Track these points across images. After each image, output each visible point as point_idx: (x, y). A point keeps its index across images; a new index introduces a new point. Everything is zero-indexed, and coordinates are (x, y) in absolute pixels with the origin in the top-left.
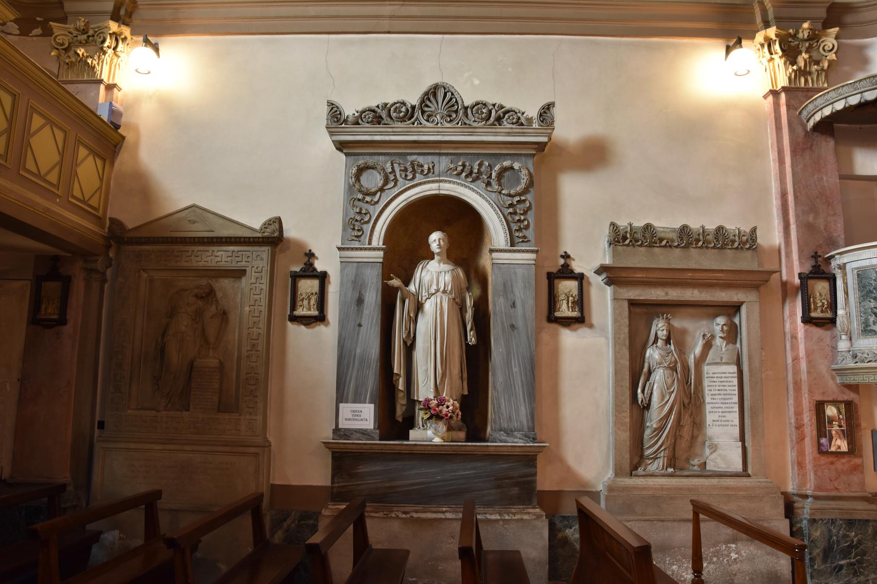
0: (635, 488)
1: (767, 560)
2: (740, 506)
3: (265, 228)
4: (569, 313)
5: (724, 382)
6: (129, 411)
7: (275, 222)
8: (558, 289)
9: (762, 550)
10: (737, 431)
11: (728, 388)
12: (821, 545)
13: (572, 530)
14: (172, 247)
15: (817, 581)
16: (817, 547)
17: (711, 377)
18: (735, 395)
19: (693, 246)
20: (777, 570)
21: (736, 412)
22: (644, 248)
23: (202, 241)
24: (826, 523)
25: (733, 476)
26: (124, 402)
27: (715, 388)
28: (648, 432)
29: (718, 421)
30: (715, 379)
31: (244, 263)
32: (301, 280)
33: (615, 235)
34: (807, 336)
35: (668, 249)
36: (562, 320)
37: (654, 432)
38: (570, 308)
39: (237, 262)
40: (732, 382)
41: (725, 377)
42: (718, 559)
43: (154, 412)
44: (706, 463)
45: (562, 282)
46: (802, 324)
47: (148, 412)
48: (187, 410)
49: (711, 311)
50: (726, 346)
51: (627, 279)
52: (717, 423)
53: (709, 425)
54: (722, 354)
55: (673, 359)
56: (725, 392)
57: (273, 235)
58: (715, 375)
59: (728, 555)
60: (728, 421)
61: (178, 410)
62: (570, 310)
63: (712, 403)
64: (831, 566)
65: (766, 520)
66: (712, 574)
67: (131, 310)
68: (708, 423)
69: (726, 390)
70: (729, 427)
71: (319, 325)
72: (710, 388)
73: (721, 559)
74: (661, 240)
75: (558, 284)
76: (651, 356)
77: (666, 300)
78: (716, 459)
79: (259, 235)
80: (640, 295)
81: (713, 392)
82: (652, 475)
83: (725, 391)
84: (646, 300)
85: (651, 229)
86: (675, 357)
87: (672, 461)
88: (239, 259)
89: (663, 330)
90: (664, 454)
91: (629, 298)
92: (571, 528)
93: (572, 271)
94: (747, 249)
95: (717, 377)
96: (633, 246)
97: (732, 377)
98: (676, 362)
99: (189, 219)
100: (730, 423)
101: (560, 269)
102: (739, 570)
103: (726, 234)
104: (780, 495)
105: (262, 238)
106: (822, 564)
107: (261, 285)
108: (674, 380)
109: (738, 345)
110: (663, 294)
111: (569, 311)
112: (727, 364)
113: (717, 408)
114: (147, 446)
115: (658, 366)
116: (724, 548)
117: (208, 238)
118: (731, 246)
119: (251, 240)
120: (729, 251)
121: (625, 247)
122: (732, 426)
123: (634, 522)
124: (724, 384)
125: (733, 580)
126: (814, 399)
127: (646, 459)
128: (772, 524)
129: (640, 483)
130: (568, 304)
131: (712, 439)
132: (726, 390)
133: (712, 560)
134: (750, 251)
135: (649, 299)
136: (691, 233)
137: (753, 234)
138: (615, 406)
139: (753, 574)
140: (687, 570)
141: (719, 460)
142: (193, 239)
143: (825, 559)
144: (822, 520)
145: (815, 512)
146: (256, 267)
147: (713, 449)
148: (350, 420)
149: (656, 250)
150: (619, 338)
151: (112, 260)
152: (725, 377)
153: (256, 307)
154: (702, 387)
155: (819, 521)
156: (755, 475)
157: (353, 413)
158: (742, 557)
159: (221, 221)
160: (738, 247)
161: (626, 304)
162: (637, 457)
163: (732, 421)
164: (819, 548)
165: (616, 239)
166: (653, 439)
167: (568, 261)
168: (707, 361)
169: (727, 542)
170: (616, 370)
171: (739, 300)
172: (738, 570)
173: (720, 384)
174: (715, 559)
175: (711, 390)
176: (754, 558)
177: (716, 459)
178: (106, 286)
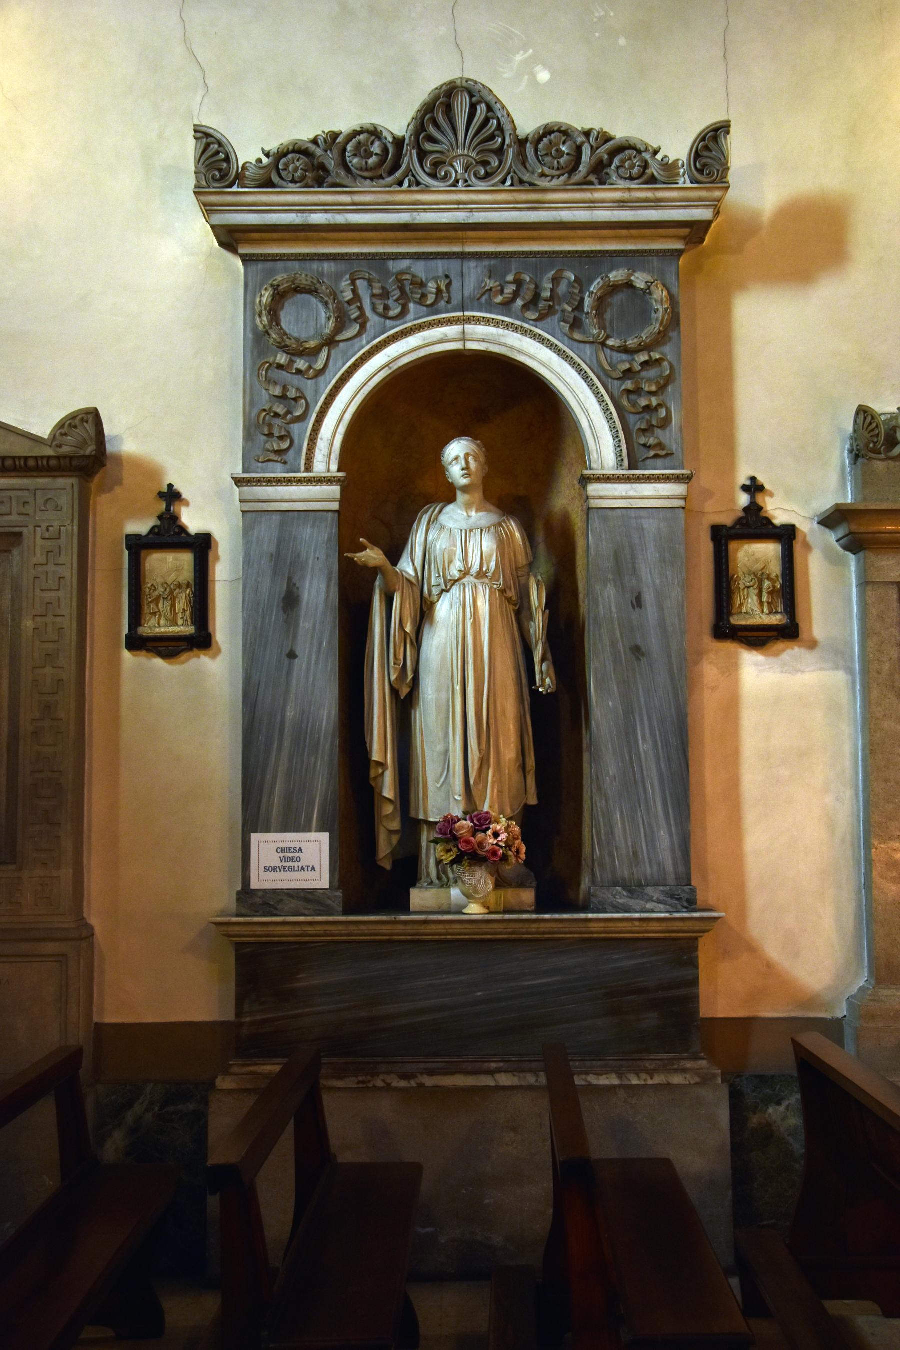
7: (87, 422)
8: (736, 559)
13: (782, 1109)
31: (14, 518)
45: (746, 547)
79: (49, 452)
92: (779, 1104)
93: (768, 521)
101: (741, 519)
111: (763, 612)
121: (890, 462)
130: (760, 596)
146: (44, 526)
148: (274, 869)
150: (879, 673)
153: (50, 619)
157: (282, 855)
165: (871, 446)
167: (760, 499)
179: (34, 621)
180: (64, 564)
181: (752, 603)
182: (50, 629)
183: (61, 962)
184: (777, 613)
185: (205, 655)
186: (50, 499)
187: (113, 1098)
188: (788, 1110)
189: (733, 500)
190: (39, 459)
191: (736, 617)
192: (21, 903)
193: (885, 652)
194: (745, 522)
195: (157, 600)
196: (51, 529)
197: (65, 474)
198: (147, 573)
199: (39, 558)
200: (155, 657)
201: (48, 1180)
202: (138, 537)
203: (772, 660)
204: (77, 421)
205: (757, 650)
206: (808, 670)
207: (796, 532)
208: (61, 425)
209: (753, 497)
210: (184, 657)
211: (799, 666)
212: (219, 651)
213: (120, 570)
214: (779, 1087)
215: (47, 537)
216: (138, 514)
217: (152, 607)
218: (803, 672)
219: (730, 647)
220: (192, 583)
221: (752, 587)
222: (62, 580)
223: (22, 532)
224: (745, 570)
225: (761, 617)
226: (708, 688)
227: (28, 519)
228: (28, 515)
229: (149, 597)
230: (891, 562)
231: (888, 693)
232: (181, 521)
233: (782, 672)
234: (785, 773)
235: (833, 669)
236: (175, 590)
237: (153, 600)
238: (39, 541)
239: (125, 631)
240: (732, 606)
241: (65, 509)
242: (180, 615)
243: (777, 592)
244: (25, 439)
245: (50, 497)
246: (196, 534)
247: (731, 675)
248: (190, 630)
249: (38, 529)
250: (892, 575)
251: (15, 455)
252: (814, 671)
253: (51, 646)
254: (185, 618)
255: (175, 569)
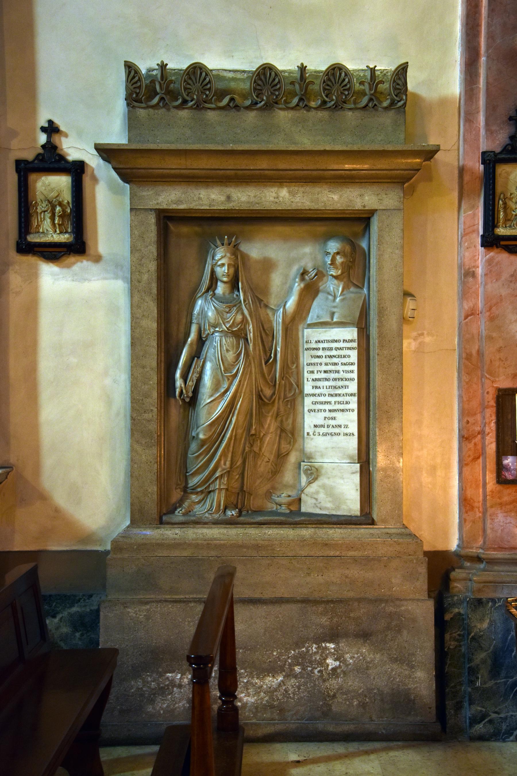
0: (160, 545)
1: (392, 670)
2: (346, 577)
4: (55, 236)
5: (335, 356)
8: (35, 188)
9: (382, 655)
10: (352, 444)
11: (340, 368)
12: (490, 645)
13: (56, 620)
15: (479, 708)
16: (481, 648)
17: (314, 349)
18: (352, 380)
19: (280, 106)
20: (409, 689)
21: (353, 410)
22: (186, 111)
24: (500, 606)
25: (342, 524)
27: (319, 368)
28: (194, 446)
29: (323, 426)
30: (320, 353)
33: (132, 88)
34: (491, 271)
35: (233, 113)
37: (202, 446)
38: (57, 226)
40: (349, 356)
41: (337, 349)
42: (303, 669)
44: (300, 500)
45: (43, 178)
46: (483, 248)
49: (321, 228)
50: (343, 291)
51: (151, 170)
52: (322, 430)
53: (308, 434)
54: (335, 307)
55: (239, 317)
56: (336, 376)
58: (321, 345)
59: (322, 663)
60: (340, 426)
62: (58, 232)
63: (314, 395)
64: (505, 683)
65: (392, 601)
66: (291, 695)
68: (307, 430)
69: (338, 372)
70: (341, 437)
72: (311, 368)
73: (309, 669)
74: (221, 94)
75: (35, 181)
76: (202, 312)
77: (227, 210)
78: (317, 493)
80: (179, 201)
81: (316, 376)
82: (198, 523)
83: (337, 374)
84: (190, 210)
85: (270, 74)
86: (243, 314)
87: (240, 497)
89: (223, 265)
90: (220, 485)
91: (158, 207)
92: (54, 617)
93: (62, 158)
94: (386, 108)
95: (324, 349)
96: (165, 106)
97: (349, 349)
98: (244, 320)
100: (343, 430)
101: (39, 154)
102: (340, 688)
103: (347, 80)
104: (421, 556)
106: (491, 680)
108: (239, 355)
109: (365, 290)
110: (223, 198)
111: (56, 231)
112: (341, 324)
113: (322, 403)
115: (212, 330)
116: (314, 650)
118: (355, 103)
120: (350, 113)
121: (151, 110)
122: (347, 434)
123: (154, 604)
124: (335, 360)
125: (330, 706)
126: (495, 386)
127: (192, 493)
128: (403, 608)
129: (172, 536)
130: (53, 218)
131: (312, 458)
132: (338, 372)
133: (292, 670)
134: (391, 113)
135: (197, 208)
136: (277, 80)
137: (399, 79)
138: (132, 402)
139: (366, 696)
140: (247, 689)
141: (322, 496)
143: (495, 672)
144: (493, 600)
145: (484, 587)
147: (313, 477)
149: (211, 115)
150: (139, 282)
152: (337, 349)
154: (297, 367)
155: (488, 602)
156: (384, 521)
158: (347, 666)
160: (367, 105)
161: (152, 219)
162: (179, 490)
163: (346, 426)
164: (486, 651)
165: (134, 96)
166: (202, 457)
167: (56, 139)
168: (309, 321)
169: (319, 640)
170: (133, 338)
171: (364, 206)
172: (338, 689)
173: (328, 360)
174: (297, 669)
175: (312, 372)
176: (368, 668)
177: (317, 493)
181: (47, 224)
184: (66, 232)
188: (61, 622)
189: (35, 140)
191: (32, 236)
193: (144, 265)
202: (26, 162)
203: (65, 271)
205: (53, 263)
206: (93, 279)
207: (85, 167)
209: (49, 137)
211: (87, 276)
214: (54, 604)
218: (90, 280)
219: (31, 259)
221: (47, 211)
224: (42, 197)
225: (52, 236)
226: (13, 293)
230: (151, 192)
231: (146, 298)
233: (73, 281)
234: (73, 360)
235: (114, 279)
240: (31, 227)
243: (68, 215)
246: (73, 161)
247: (32, 282)
250: (151, 203)
252: (98, 280)
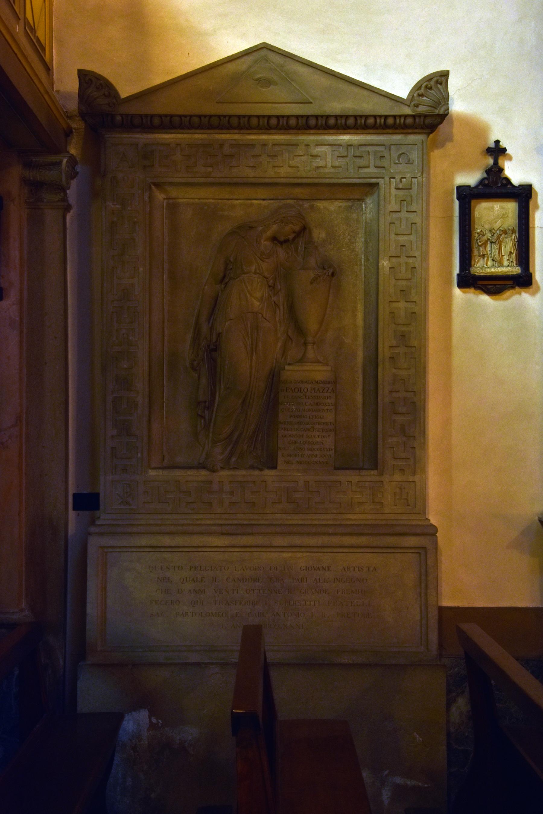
3: (419, 95)
6: (152, 473)
7: (441, 84)
14: (217, 136)
23: (285, 123)
26: (139, 455)
31: (372, 170)
32: (480, 203)
36: (486, 283)
39: (360, 167)
43: (203, 472)
47: (191, 472)
48: (274, 467)
57: (437, 111)
61: (252, 467)
67: (141, 269)
71: (520, 294)
79: (407, 111)
88: (362, 162)
99: (257, 76)
105: (414, 117)
107: (411, 215)
114: (197, 541)
117: (297, 117)
119: (390, 121)
142: (266, 120)
146: (398, 177)
151: (76, 163)
153: (403, 260)
159: (325, 81)
178: (69, 217)
179: (389, 261)
180: (416, 212)
182: (403, 269)
183: (420, 553)
185: (526, 292)
186: (403, 153)
187: (456, 669)
190: (397, 118)
192: (382, 503)
194: (486, 182)
195: (485, 244)
196: (404, 180)
197: (417, 131)
198: (476, 220)
199: (394, 205)
200: (481, 294)
201: (418, 737)
204: (432, 83)
208: (418, 87)
210: (508, 293)
212: (538, 289)
213: (451, 217)
215: (401, 187)
216: (467, 167)
217: (481, 250)
220: (517, 229)
222: (413, 225)
223: (378, 183)
227: (384, 171)
228: (384, 167)
229: (479, 241)
232: (504, 174)
236: (501, 235)
237: (482, 244)
238: (393, 192)
239: (456, 270)
241: (416, 163)
242: (506, 258)
244: (386, 100)
245: (403, 152)
248: (516, 270)
249: (392, 180)
251: (259, 114)
253: (404, 283)
254: (511, 260)
255: (500, 217)
